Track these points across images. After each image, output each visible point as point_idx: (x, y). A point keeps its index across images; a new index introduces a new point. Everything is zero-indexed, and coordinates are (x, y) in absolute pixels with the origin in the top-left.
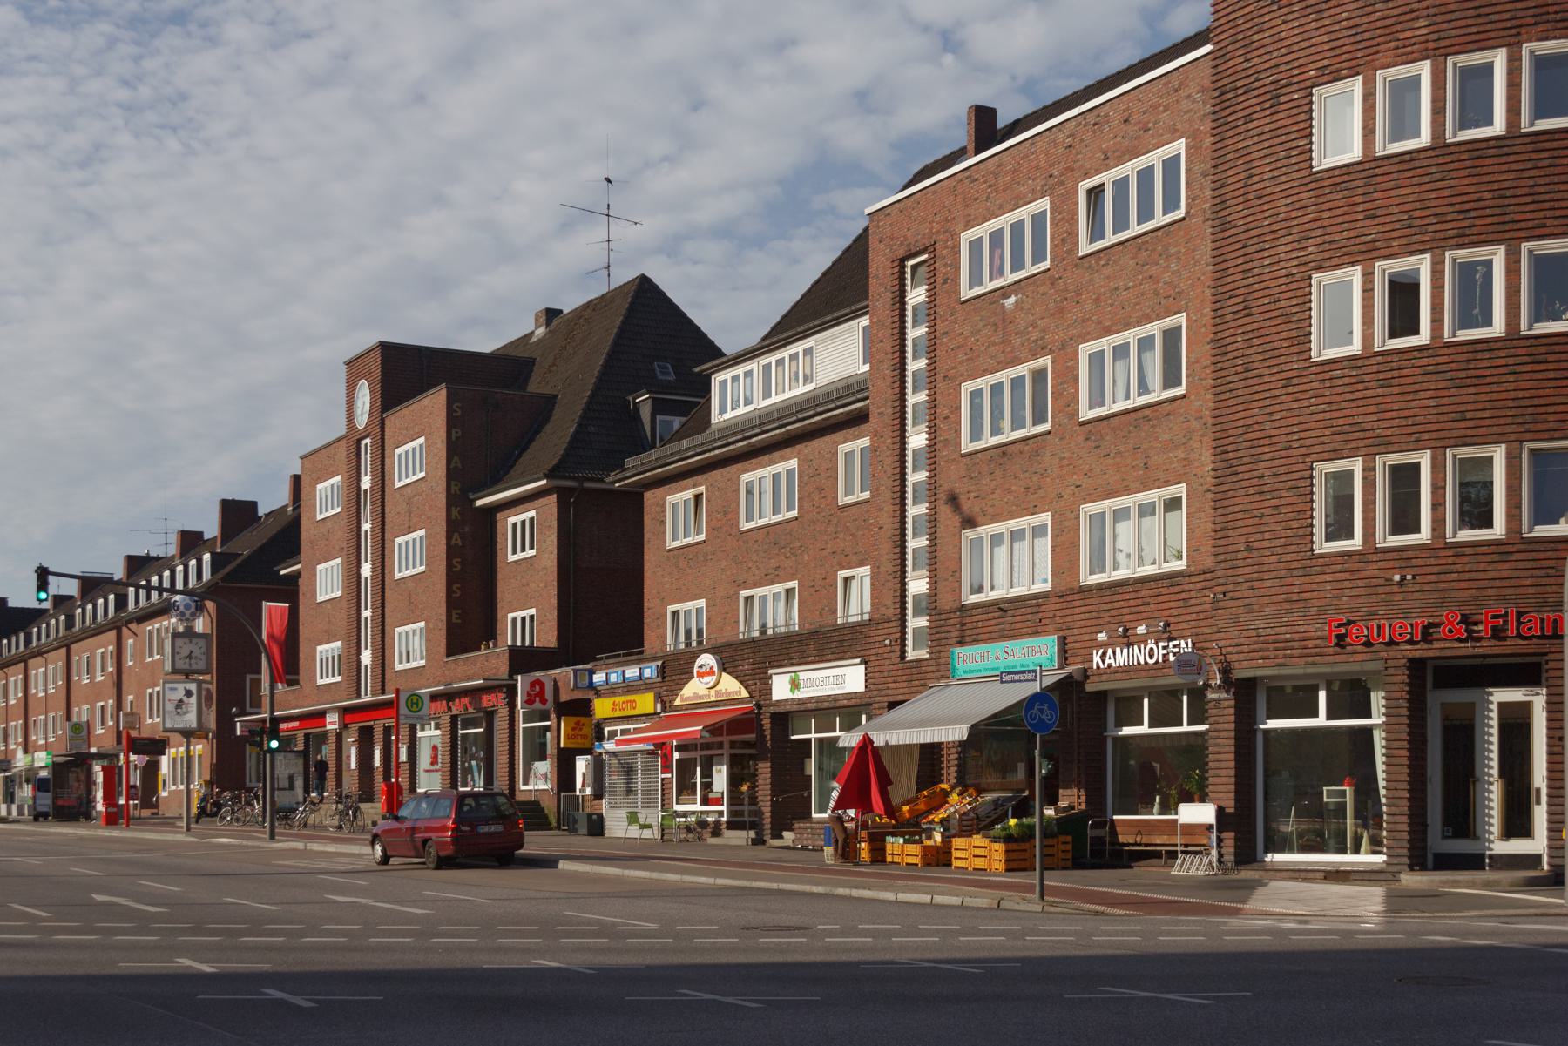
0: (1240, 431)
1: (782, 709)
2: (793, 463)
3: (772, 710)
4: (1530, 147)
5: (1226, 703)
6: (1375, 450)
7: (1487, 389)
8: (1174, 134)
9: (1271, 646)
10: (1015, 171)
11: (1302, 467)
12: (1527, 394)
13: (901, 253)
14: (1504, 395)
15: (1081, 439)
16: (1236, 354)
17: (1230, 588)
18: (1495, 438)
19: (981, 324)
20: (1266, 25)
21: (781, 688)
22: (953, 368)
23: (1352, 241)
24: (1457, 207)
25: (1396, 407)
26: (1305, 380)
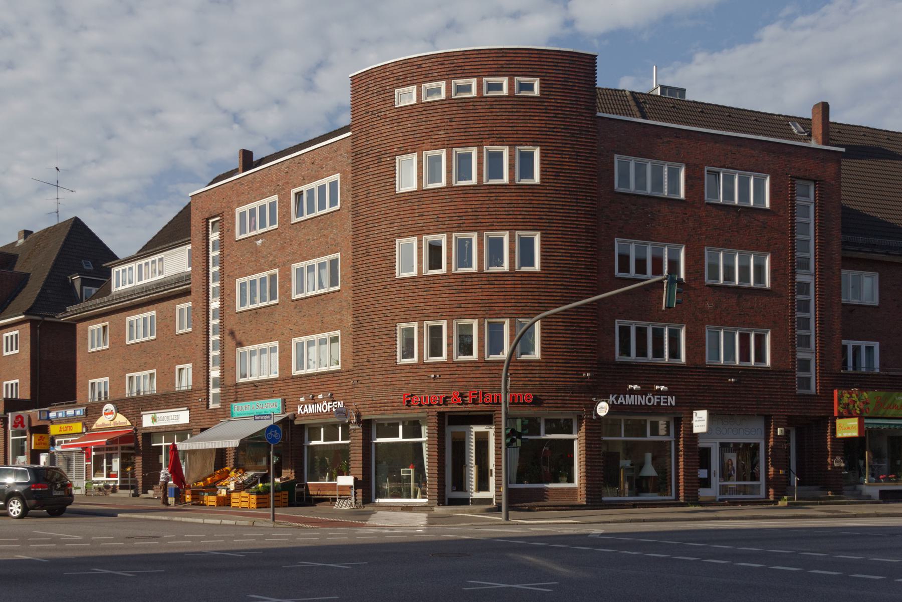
2: (153, 313)
4: (487, 191)
9: (378, 405)
10: (262, 181)
11: (392, 325)
13: (207, 216)
15: (292, 308)
17: (360, 378)
20: (375, 126)
21: (147, 421)
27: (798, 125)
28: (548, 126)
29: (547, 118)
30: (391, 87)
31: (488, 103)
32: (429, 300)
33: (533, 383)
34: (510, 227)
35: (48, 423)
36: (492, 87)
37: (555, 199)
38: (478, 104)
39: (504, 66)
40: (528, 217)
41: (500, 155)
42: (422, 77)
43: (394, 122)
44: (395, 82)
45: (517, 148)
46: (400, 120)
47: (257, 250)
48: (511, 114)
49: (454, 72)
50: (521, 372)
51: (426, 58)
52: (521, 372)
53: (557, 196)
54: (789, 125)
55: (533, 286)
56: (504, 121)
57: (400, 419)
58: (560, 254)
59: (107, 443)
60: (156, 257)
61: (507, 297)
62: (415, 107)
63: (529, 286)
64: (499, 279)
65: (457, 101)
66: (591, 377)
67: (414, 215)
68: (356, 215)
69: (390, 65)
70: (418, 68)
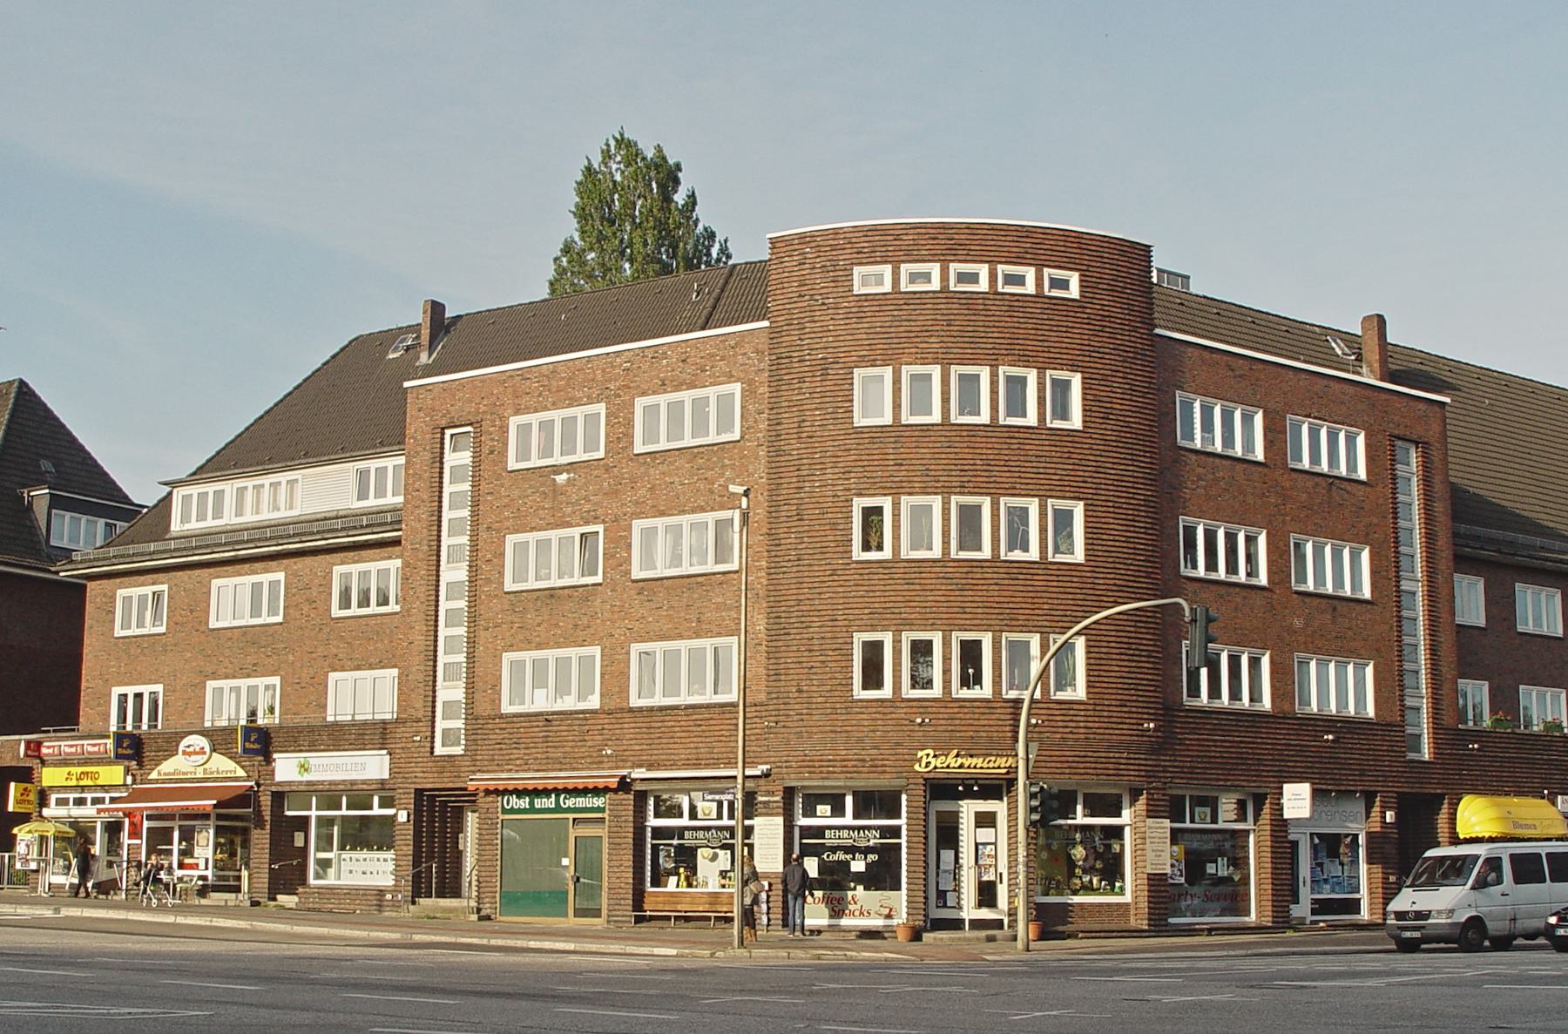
0: (792, 603)
1: (280, 789)
2: (281, 576)
3: (274, 789)
4: (1006, 435)
5: (775, 805)
6: (902, 627)
7: (980, 593)
8: (730, 378)
9: (817, 764)
10: (570, 378)
11: (845, 635)
12: (1006, 600)
13: (443, 423)
14: (992, 599)
16: (789, 546)
17: (781, 718)
18: (985, 627)
19: (530, 491)
20: (816, 319)
21: (286, 768)
22: (497, 522)
23: (885, 479)
24: (959, 467)
25: (918, 599)
26: (847, 572)
27: (1339, 341)
28: (1092, 343)
29: (1091, 333)
30: (848, 262)
31: (1007, 303)
32: (912, 598)
33: (1074, 736)
34: (1041, 493)
35: (34, 763)
36: (1011, 279)
37: (1103, 453)
38: (990, 302)
39: (1030, 251)
40: (1067, 478)
41: (1023, 381)
42: (902, 253)
43: (851, 315)
44: (855, 256)
45: (1048, 372)
46: (863, 315)
47: (556, 490)
48: (1040, 322)
49: (953, 252)
50: (1058, 718)
51: (909, 226)
52: (1058, 718)
53: (1106, 448)
54: (1327, 341)
55: (1074, 585)
56: (1031, 332)
57: (848, 788)
58: (1112, 538)
59: (215, 806)
60: (283, 477)
61: (1036, 600)
62: (888, 297)
63: (1069, 584)
64: (1025, 571)
65: (958, 295)
66: (1155, 730)
67: (886, 463)
68: (776, 454)
69: (846, 230)
70: (895, 240)
